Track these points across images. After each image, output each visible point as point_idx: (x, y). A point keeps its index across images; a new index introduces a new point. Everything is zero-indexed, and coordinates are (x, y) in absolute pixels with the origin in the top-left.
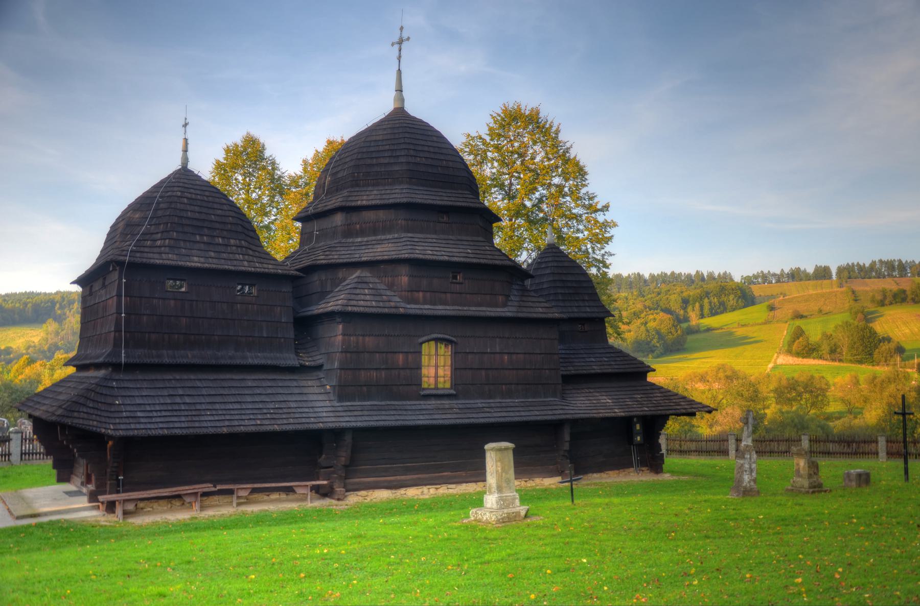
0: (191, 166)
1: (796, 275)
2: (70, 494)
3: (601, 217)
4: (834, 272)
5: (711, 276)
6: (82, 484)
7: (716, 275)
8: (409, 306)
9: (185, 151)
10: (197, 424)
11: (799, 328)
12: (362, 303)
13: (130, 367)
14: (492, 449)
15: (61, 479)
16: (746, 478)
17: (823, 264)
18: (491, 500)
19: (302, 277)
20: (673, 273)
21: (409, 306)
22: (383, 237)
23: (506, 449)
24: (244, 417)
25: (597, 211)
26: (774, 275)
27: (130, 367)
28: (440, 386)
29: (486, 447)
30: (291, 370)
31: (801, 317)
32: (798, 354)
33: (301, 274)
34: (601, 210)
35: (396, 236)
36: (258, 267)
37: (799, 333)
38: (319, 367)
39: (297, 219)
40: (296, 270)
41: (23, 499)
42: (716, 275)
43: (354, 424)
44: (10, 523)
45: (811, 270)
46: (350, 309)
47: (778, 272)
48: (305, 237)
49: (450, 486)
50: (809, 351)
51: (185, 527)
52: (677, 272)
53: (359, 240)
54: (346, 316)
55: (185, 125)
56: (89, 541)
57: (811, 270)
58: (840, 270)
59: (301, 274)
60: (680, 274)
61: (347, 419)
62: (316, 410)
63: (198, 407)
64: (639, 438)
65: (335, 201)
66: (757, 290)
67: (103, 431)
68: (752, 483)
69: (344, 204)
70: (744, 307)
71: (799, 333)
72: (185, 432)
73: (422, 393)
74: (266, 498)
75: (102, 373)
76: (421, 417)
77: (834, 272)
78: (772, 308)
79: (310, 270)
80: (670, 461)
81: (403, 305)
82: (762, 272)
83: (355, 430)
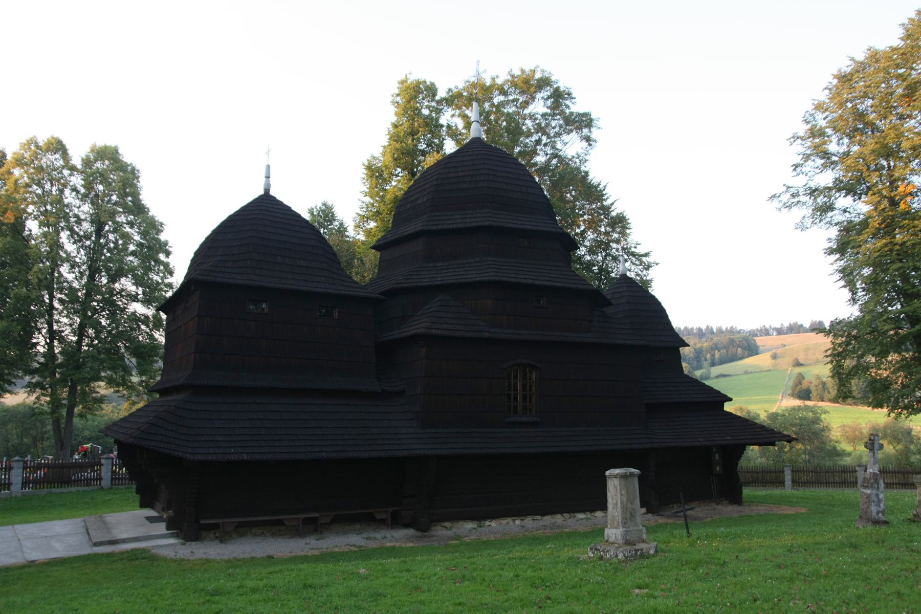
0: (271, 193)
1: (796, 329)
2: (151, 519)
5: (720, 331)
9: (268, 177)
12: (445, 326)
14: (615, 476)
15: (143, 505)
16: (874, 509)
18: (613, 533)
20: (686, 328)
21: (492, 330)
23: (632, 474)
29: (607, 473)
31: (802, 365)
33: (383, 297)
39: (373, 248)
41: (104, 523)
44: (87, 550)
45: (807, 325)
46: (434, 331)
47: (779, 326)
48: (383, 265)
49: (535, 517)
52: (689, 327)
53: (440, 264)
57: (807, 325)
59: (383, 297)
60: (692, 329)
64: (718, 468)
65: (417, 226)
66: (760, 341)
67: (181, 454)
68: (880, 515)
69: (425, 228)
75: (180, 397)
79: (392, 293)
80: (747, 492)
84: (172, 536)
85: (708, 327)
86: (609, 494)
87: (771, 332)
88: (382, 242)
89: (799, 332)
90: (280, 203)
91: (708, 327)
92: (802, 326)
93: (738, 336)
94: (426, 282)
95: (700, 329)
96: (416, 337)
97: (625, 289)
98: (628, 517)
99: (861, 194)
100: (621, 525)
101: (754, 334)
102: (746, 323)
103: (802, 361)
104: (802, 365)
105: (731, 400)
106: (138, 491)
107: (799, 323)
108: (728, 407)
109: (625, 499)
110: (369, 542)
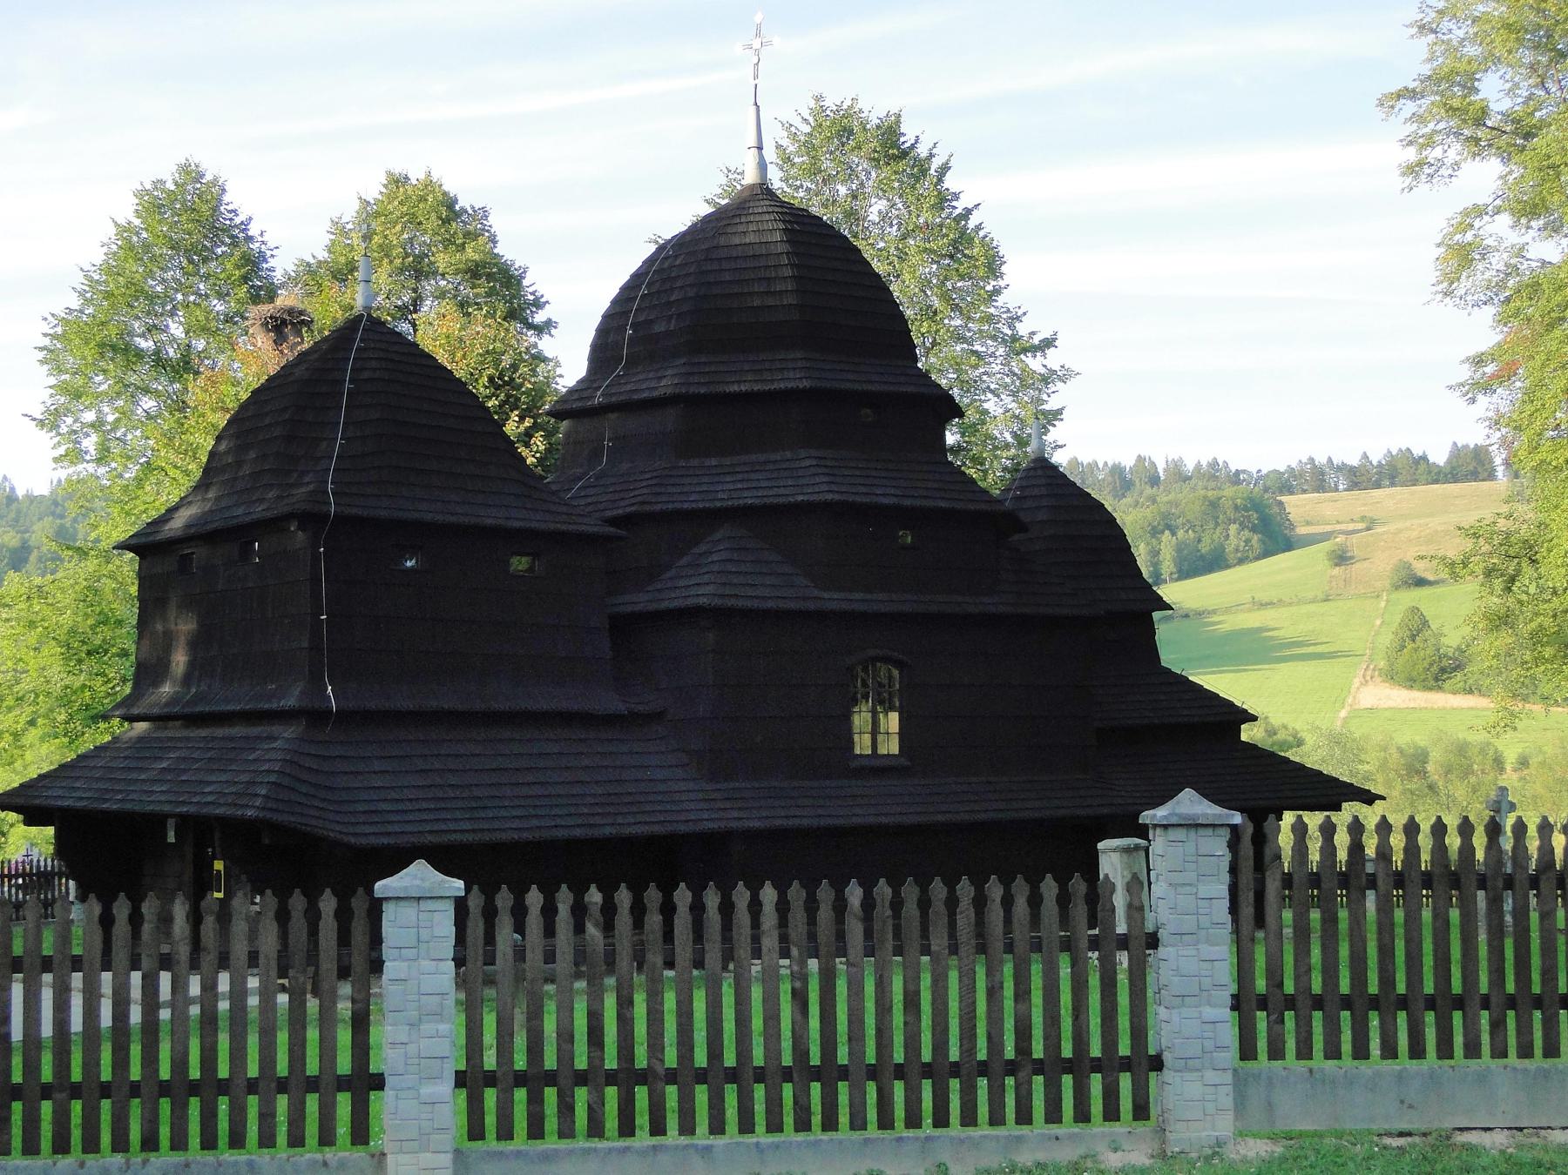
3: (1035, 363)
5: (1178, 474)
7: (1190, 466)
8: (826, 595)
11: (1415, 610)
19: (620, 538)
22: (762, 457)
24: (443, 815)
25: (1025, 351)
26: (1342, 468)
27: (346, 718)
28: (882, 750)
29: (1100, 846)
30: (610, 720)
31: (1421, 582)
32: (1411, 682)
36: (538, 521)
37: (1416, 627)
38: (658, 716)
40: (613, 522)
42: (1190, 466)
45: (1439, 457)
47: (1354, 461)
50: (1442, 671)
54: (720, 616)
57: (1439, 457)
61: (735, 814)
62: (677, 797)
63: (477, 792)
65: (666, 382)
66: (1297, 506)
70: (1267, 554)
71: (1416, 627)
72: (470, 837)
73: (854, 764)
76: (858, 811)
78: (1341, 558)
81: (816, 593)
82: (1312, 460)
83: (750, 836)
85: (1140, 459)
87: (1331, 478)
89: (1415, 483)
91: (1140, 459)
92: (1424, 458)
93: (1229, 491)
95: (1117, 470)
97: (1044, 491)
99: (1516, 314)
101: (1286, 483)
102: (1258, 452)
104: (1421, 582)
107: (1417, 452)
108: (1248, 733)
110: (793, 935)
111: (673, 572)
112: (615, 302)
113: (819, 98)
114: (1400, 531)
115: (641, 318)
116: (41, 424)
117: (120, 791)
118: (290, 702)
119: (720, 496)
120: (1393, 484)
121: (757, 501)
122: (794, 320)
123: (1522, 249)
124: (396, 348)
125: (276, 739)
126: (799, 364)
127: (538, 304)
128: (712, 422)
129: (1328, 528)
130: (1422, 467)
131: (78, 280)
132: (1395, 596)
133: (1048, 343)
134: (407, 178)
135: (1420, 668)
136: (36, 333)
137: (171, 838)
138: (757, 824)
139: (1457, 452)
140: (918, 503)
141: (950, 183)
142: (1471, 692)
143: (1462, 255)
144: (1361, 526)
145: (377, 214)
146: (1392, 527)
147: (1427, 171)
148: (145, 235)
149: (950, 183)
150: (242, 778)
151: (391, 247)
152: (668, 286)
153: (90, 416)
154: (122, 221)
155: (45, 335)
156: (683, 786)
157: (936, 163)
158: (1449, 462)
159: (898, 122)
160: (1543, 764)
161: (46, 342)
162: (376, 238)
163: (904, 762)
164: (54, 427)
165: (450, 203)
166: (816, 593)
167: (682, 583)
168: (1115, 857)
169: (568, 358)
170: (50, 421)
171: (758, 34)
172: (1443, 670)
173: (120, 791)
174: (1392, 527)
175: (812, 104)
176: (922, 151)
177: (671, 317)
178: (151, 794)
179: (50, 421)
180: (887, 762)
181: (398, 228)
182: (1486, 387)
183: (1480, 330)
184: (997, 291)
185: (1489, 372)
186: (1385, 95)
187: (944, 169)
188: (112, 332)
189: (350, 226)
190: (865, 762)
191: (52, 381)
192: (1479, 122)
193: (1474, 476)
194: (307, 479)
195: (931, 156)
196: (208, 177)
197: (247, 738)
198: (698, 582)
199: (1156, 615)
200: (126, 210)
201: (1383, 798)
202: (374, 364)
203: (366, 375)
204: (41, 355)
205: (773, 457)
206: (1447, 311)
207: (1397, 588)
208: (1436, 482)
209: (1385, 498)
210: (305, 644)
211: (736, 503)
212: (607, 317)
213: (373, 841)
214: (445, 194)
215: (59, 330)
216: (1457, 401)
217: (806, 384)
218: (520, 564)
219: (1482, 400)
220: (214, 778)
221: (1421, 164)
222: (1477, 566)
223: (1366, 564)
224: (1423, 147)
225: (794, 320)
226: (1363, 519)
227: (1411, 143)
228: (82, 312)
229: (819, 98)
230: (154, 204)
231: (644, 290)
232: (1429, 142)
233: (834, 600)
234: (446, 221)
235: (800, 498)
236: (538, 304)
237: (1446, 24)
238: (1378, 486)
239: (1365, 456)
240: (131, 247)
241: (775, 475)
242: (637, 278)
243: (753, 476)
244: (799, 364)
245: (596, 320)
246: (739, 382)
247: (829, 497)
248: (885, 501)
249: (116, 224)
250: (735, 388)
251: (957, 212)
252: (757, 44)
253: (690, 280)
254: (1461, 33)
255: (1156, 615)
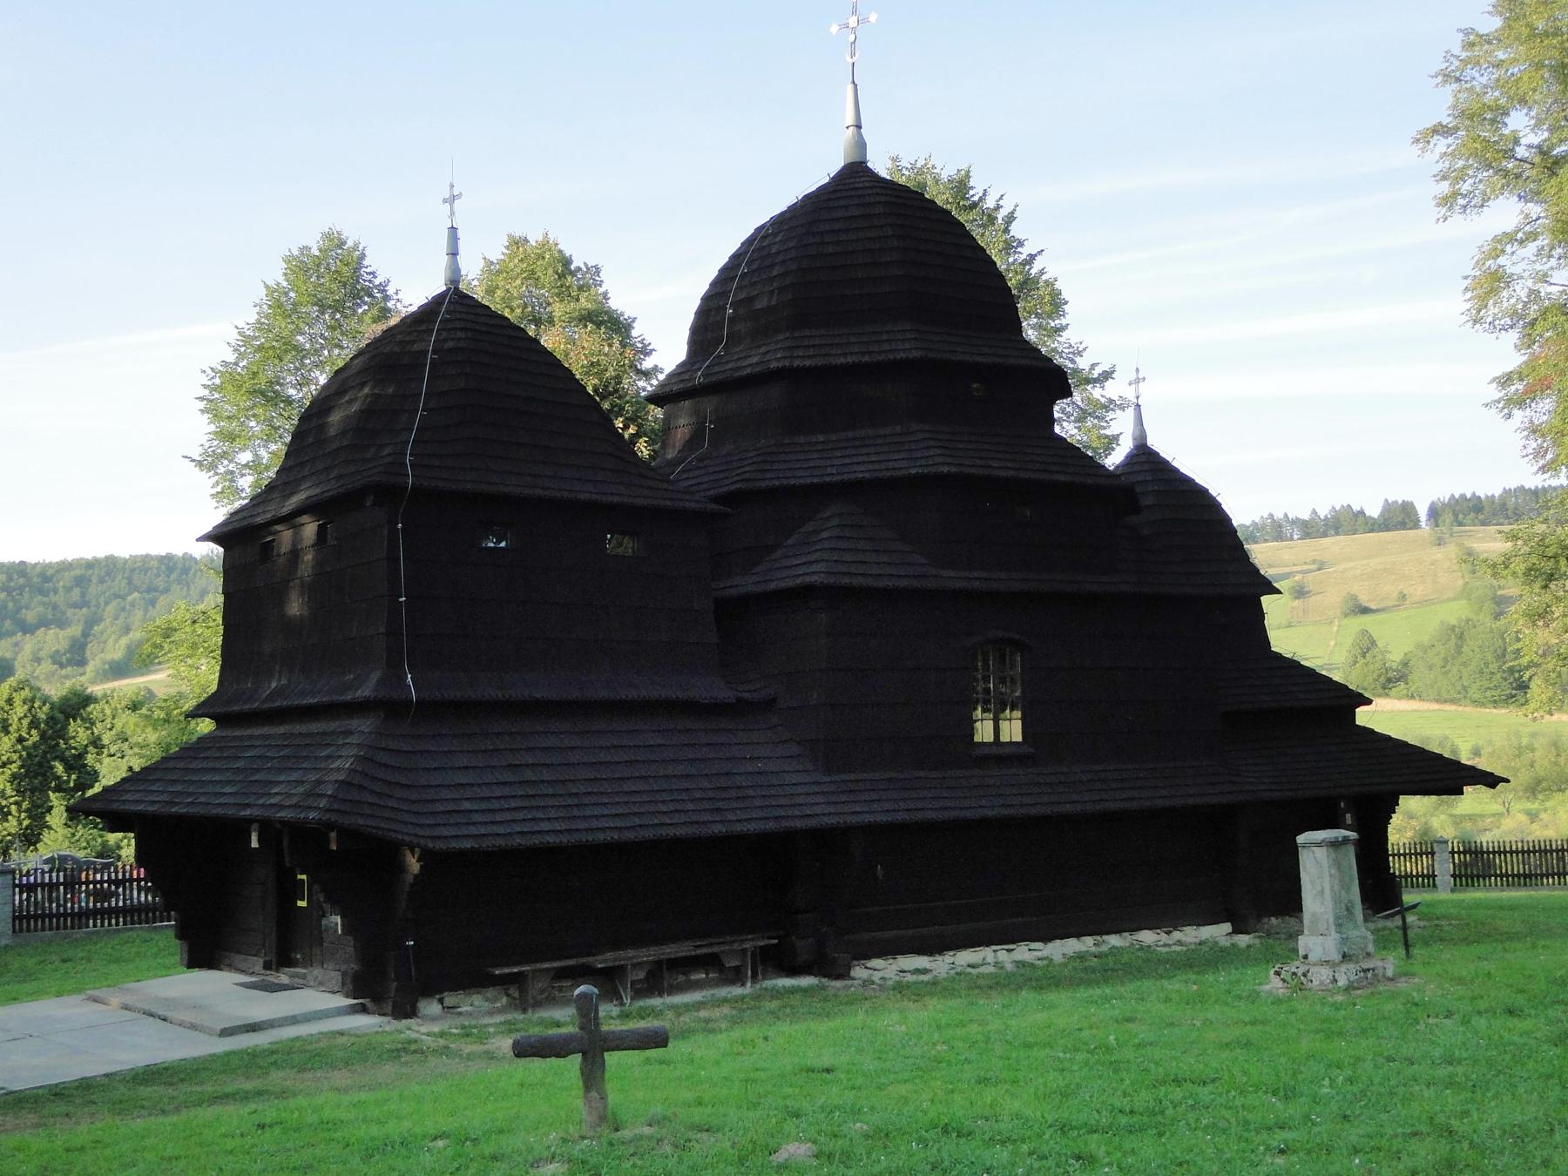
4: (1423, 512)
6: (267, 966)
9: (453, 253)
10: (582, 825)
11: (1364, 632)
13: (431, 710)
17: (1399, 497)
23: (1346, 840)
26: (1297, 522)
27: (431, 710)
28: (1005, 738)
29: (1300, 839)
30: (715, 709)
31: (1365, 611)
34: (1095, 381)
35: (898, 429)
38: (768, 704)
40: (715, 499)
43: (868, 818)
45: (1374, 511)
47: (1305, 516)
51: (1002, 983)
55: (451, 200)
56: (963, 993)
57: (1374, 511)
58: (1435, 513)
74: (681, 978)
77: (1423, 512)
80: (1408, 898)
81: (933, 571)
82: (1271, 516)
84: (363, 1009)
86: (1303, 875)
87: (1287, 530)
88: (667, 389)
90: (1188, 481)
92: (1362, 512)
94: (804, 478)
96: (805, 593)
98: (1342, 921)
100: (1333, 929)
103: (1365, 600)
104: (1365, 611)
105: (1368, 702)
106: (182, 933)
107: (1356, 508)
108: (1363, 716)
109: (1337, 888)
111: (779, 553)
112: (714, 284)
113: (895, 159)
114: (1345, 570)
115: (742, 296)
116: (200, 464)
117: (191, 794)
118: (365, 692)
119: (829, 470)
120: (1337, 534)
121: (867, 475)
122: (887, 298)
123: (1546, 275)
124: (484, 319)
125: (351, 733)
126: (908, 335)
127: (646, 351)
128: (816, 396)
129: (1287, 570)
130: (1361, 519)
131: (233, 336)
132: (1346, 621)
133: (1107, 375)
134: (526, 240)
135: (1370, 679)
136: (196, 386)
137: (255, 844)
138: (880, 818)
139: (1388, 507)
140: (1033, 476)
141: (1016, 230)
142: (1413, 697)
143: (1490, 283)
144: (1314, 567)
145: (499, 272)
146: (1341, 567)
147: (1461, 201)
148: (292, 294)
149: (1016, 230)
150: (306, 781)
151: (511, 298)
152: (768, 262)
153: (245, 457)
154: (272, 283)
155: (205, 386)
156: (795, 778)
157: (1001, 215)
158: (1382, 514)
159: (968, 176)
160: (1492, 754)
161: (206, 392)
162: (499, 292)
163: (1026, 749)
164: (212, 467)
165: (567, 262)
166: (933, 571)
167: (788, 562)
168: (1321, 853)
169: (667, 347)
170: (207, 463)
171: (854, 12)
172: (1389, 680)
173: (191, 794)
174: (1341, 567)
175: (889, 164)
176: (990, 203)
177: (772, 292)
178: (217, 796)
179: (207, 463)
180: (1007, 751)
181: (518, 282)
182: (1520, 402)
183: (1506, 353)
184: (1059, 330)
185: (1519, 390)
186: (1419, 132)
187: (1010, 218)
188: (262, 381)
189: (475, 283)
190: (987, 751)
191: (212, 428)
192: (1509, 154)
193: (1403, 526)
194: (386, 452)
195: (998, 207)
196: (350, 243)
197: (324, 733)
198: (812, 558)
199: (1266, 600)
200: (276, 274)
201: (1507, 781)
202: (460, 334)
203: (450, 344)
204: (202, 405)
205: (881, 432)
206: (1480, 336)
207: (1346, 615)
208: (1372, 531)
209: (1331, 545)
210: (382, 630)
211: (846, 477)
212: (707, 299)
213: (455, 844)
214: (560, 252)
215: (217, 381)
216: (1494, 415)
217: (915, 354)
218: (618, 545)
219: (1518, 414)
220: (282, 778)
221: (1455, 194)
222: (1519, 567)
223: (1319, 597)
224: (1457, 180)
225: (887, 298)
226: (1314, 561)
227: (1444, 178)
228: (236, 364)
229: (895, 159)
230: (301, 266)
231: (743, 269)
232: (1461, 176)
233: (952, 578)
234: (561, 276)
235: (913, 471)
236: (646, 351)
237: (1469, 72)
238: (1325, 535)
239: (1314, 512)
240: (280, 305)
241: (885, 449)
242: (736, 258)
243: (864, 451)
244: (908, 335)
245: (695, 304)
246: (845, 355)
247: (945, 469)
248: (1003, 473)
249: (267, 287)
250: (842, 360)
251: (1023, 257)
252: (853, 22)
253: (793, 254)
254: (1484, 80)
255: (1266, 600)
